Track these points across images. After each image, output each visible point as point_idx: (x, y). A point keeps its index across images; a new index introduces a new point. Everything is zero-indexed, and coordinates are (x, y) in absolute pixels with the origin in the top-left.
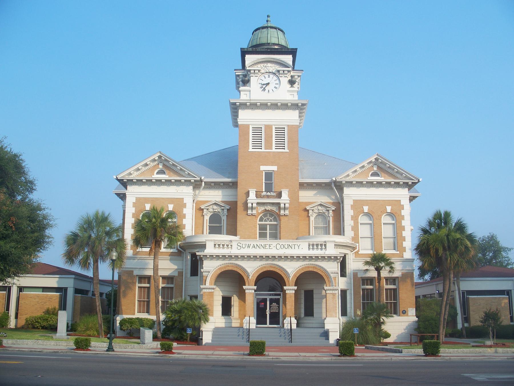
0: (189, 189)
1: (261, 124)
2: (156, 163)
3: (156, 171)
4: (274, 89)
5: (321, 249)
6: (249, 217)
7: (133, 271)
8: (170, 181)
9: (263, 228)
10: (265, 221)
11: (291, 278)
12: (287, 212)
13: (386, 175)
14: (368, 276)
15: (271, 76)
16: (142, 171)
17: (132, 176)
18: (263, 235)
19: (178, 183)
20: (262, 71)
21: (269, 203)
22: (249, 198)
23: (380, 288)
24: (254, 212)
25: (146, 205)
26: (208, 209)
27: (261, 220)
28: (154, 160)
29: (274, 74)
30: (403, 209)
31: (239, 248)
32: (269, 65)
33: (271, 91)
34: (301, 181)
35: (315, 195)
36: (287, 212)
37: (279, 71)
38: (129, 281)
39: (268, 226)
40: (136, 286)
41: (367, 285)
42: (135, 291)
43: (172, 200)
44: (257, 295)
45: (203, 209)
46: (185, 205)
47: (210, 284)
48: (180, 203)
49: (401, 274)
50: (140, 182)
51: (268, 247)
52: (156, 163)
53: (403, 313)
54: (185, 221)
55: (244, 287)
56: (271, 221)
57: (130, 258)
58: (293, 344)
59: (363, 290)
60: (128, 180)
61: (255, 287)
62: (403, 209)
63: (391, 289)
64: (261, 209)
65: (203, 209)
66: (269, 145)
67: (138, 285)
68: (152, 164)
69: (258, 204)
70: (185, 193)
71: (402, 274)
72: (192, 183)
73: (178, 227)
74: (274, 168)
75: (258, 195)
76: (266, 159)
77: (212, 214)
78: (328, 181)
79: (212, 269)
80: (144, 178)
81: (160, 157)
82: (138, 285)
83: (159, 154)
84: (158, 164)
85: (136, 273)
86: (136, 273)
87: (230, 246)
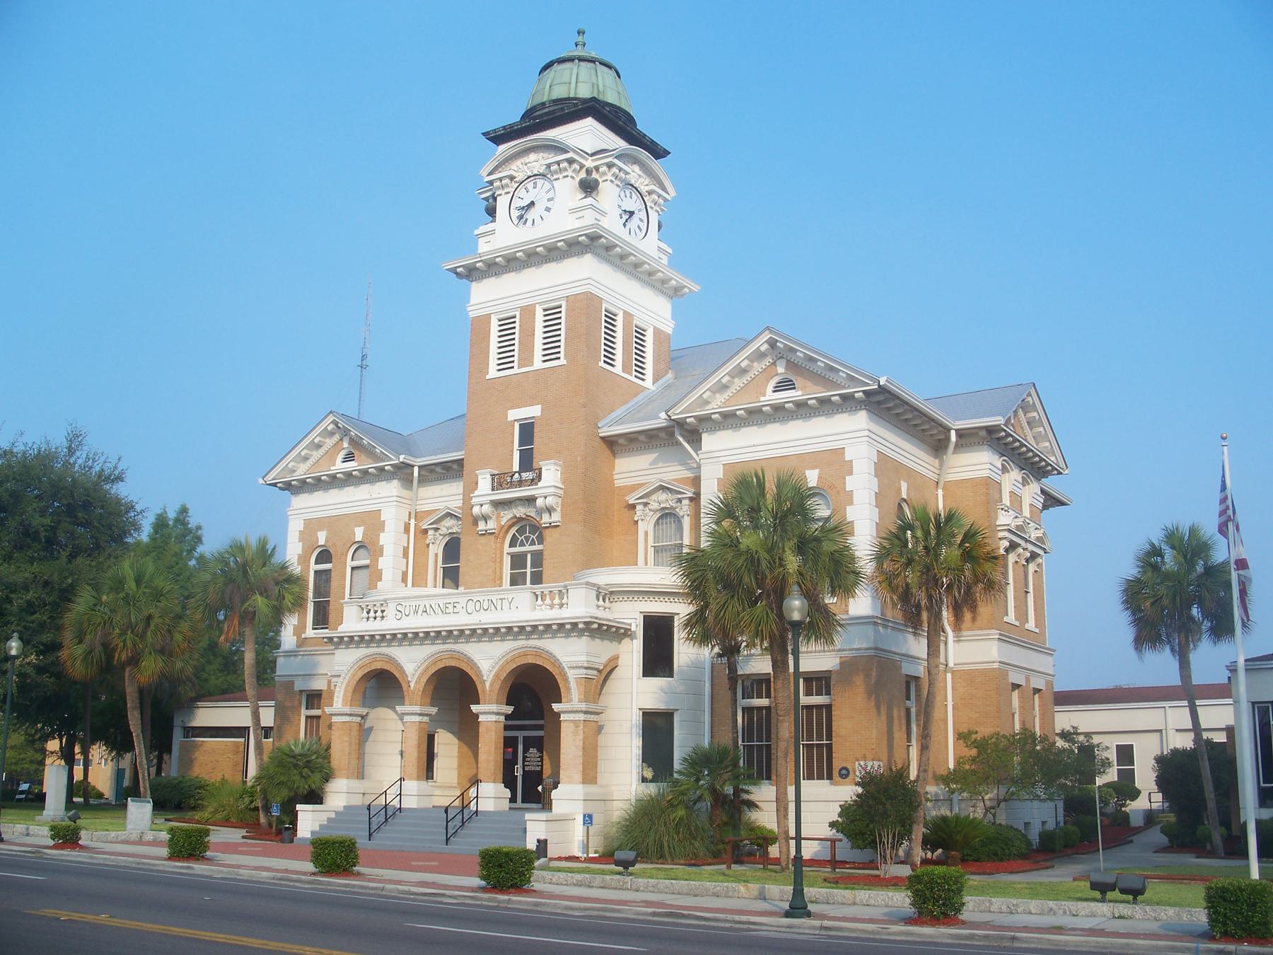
0: (391, 489)
1: (512, 307)
2: (769, 360)
3: (772, 383)
4: (545, 214)
5: (552, 606)
6: (483, 540)
7: (293, 683)
8: (365, 472)
9: (518, 561)
10: (522, 544)
11: (488, 685)
12: (556, 517)
13: (809, 384)
14: (754, 671)
15: (540, 182)
16: (732, 390)
17: (710, 406)
18: (516, 580)
19: (825, 406)
20: (520, 177)
21: (520, 499)
22: (476, 493)
23: (784, 702)
24: (491, 525)
25: (817, 471)
26: (646, 504)
27: (512, 544)
28: (759, 356)
29: (543, 175)
30: (851, 473)
31: (399, 615)
32: (533, 157)
33: (538, 221)
34: (606, 432)
35: (654, 462)
36: (556, 517)
37: (549, 166)
38: (288, 704)
39: (529, 556)
40: (299, 715)
41: (760, 696)
42: (299, 724)
43: (815, 459)
44: (506, 728)
45: (633, 507)
46: (848, 468)
47: (344, 704)
48: (836, 461)
49: (837, 661)
50: (729, 420)
51: (451, 609)
52: (769, 360)
53: (842, 776)
54: (852, 513)
55: (474, 708)
56: (533, 543)
57: (290, 654)
58: (452, 847)
59: (748, 710)
60: (701, 419)
61: (510, 710)
62: (851, 473)
63: (819, 707)
64: (507, 516)
65: (633, 507)
66: (527, 359)
67: (304, 712)
68: (330, 442)
69: (497, 504)
70: (385, 498)
71: (841, 663)
72: (860, 402)
73: (835, 529)
74: (534, 411)
75: (499, 482)
76: (515, 391)
77: (447, 539)
78: (661, 421)
79: (344, 668)
80: (740, 407)
81: (772, 344)
82: (304, 712)
83: (767, 336)
84: (774, 364)
85: (298, 686)
86: (298, 686)
87: (379, 614)
